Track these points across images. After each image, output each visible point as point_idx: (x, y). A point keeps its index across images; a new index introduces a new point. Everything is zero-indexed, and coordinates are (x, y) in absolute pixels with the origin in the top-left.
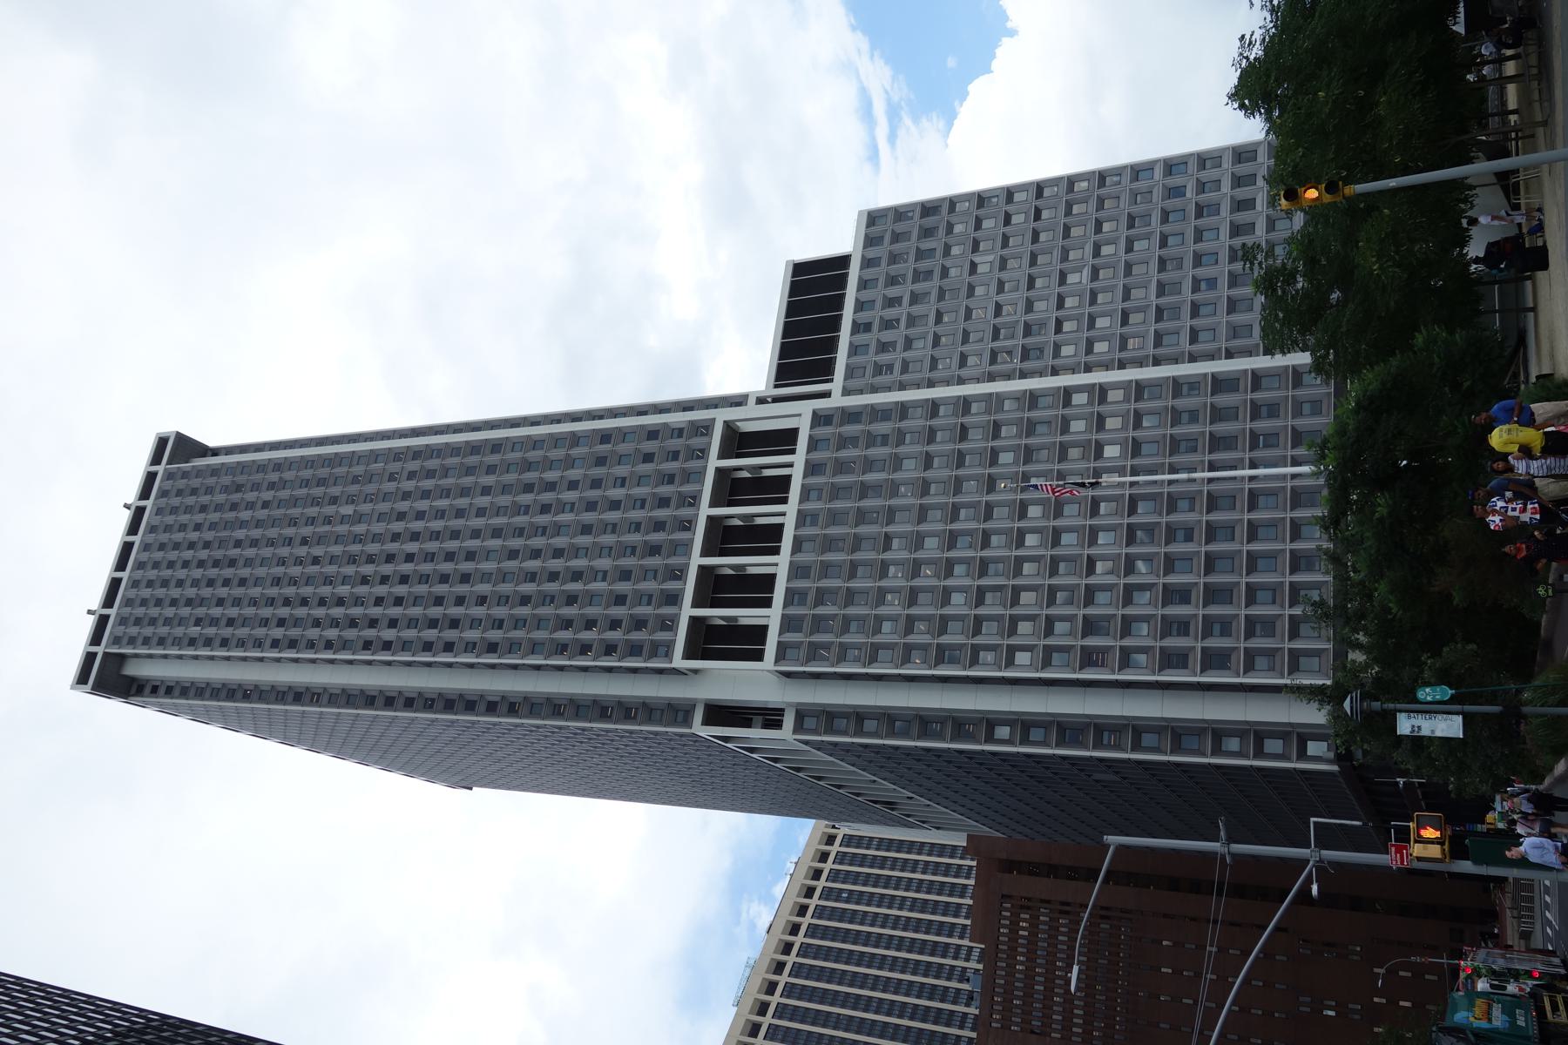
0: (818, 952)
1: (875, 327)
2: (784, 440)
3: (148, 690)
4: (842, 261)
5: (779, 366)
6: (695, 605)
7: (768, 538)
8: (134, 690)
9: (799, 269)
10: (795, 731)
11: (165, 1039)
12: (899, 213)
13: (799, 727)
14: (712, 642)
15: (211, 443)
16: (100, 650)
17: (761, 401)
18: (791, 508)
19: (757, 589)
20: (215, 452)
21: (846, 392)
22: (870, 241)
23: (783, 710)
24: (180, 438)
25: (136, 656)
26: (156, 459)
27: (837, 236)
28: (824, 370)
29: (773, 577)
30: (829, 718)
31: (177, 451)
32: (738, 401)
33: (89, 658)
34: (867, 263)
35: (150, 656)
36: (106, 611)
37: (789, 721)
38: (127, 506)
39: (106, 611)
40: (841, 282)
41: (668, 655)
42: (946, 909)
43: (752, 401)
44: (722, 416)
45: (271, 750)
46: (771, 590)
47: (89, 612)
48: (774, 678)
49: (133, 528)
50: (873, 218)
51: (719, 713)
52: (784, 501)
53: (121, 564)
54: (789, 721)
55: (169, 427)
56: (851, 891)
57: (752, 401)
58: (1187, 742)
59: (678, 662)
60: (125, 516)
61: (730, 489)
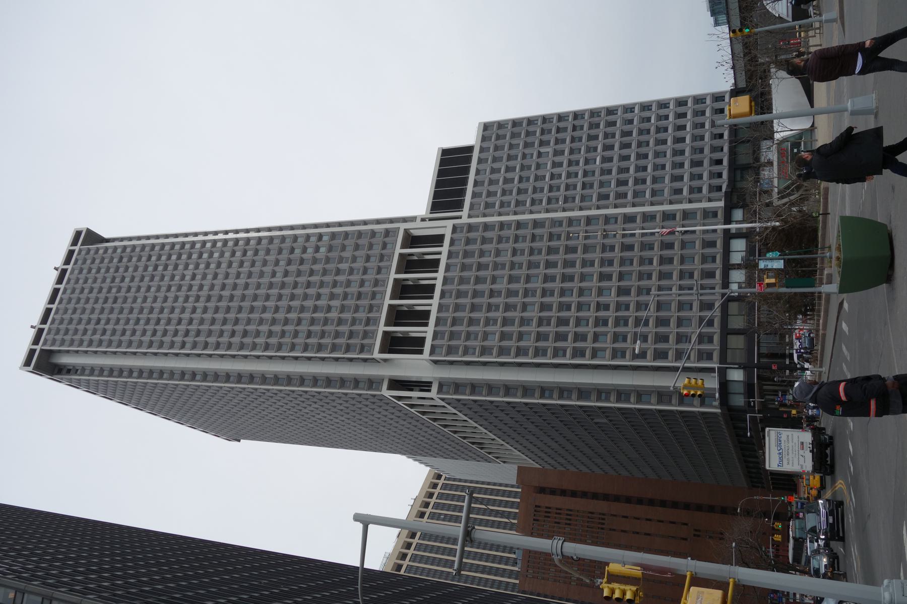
0: (426, 548)
1: (486, 183)
2: (437, 240)
3: (64, 371)
4: (469, 149)
5: (435, 192)
6: (386, 325)
7: (422, 317)
8: (56, 371)
9: (445, 152)
10: (438, 393)
11: (163, 601)
12: (501, 125)
13: (440, 391)
14: (393, 344)
15: (106, 236)
16: (38, 348)
17: (423, 220)
18: (435, 301)
19: (422, 317)
20: (108, 241)
21: (470, 216)
22: (484, 139)
23: (431, 383)
24: (89, 232)
25: (59, 351)
26: (75, 242)
27: (467, 136)
28: (459, 206)
29: (424, 339)
30: (458, 386)
31: (89, 238)
32: (413, 219)
33: (32, 352)
34: (482, 150)
35: (68, 352)
36: (42, 326)
37: (435, 388)
38: (56, 269)
39: (42, 326)
40: (469, 160)
41: (371, 351)
42: (506, 505)
43: (418, 220)
44: (403, 226)
45: (158, 422)
46: (423, 345)
47: (32, 327)
48: (427, 364)
49: (60, 280)
50: (486, 127)
51: (396, 384)
52: (431, 298)
53: (52, 300)
54: (435, 388)
55: (83, 225)
56: (445, 515)
57: (418, 220)
58: (644, 398)
59: (376, 355)
60: (55, 275)
61: (407, 264)
